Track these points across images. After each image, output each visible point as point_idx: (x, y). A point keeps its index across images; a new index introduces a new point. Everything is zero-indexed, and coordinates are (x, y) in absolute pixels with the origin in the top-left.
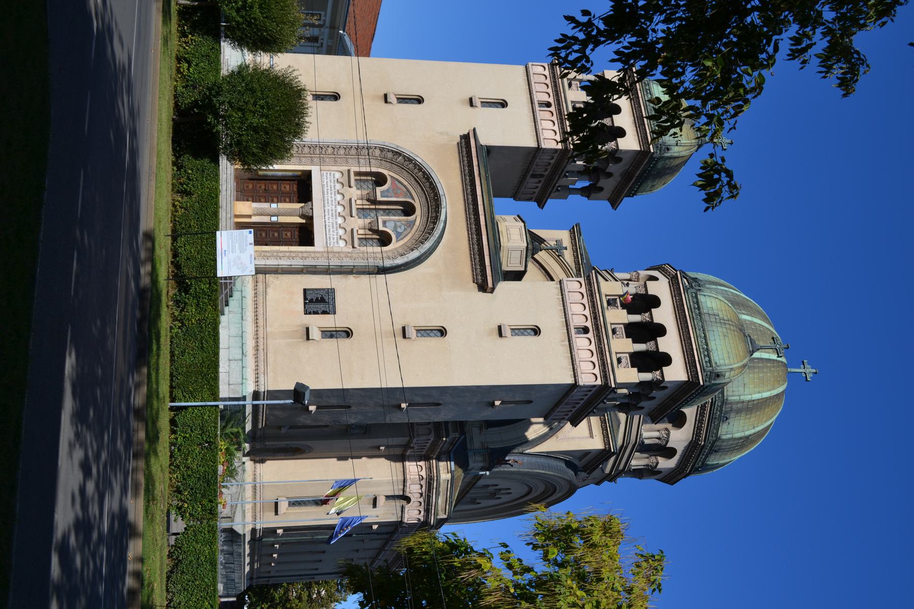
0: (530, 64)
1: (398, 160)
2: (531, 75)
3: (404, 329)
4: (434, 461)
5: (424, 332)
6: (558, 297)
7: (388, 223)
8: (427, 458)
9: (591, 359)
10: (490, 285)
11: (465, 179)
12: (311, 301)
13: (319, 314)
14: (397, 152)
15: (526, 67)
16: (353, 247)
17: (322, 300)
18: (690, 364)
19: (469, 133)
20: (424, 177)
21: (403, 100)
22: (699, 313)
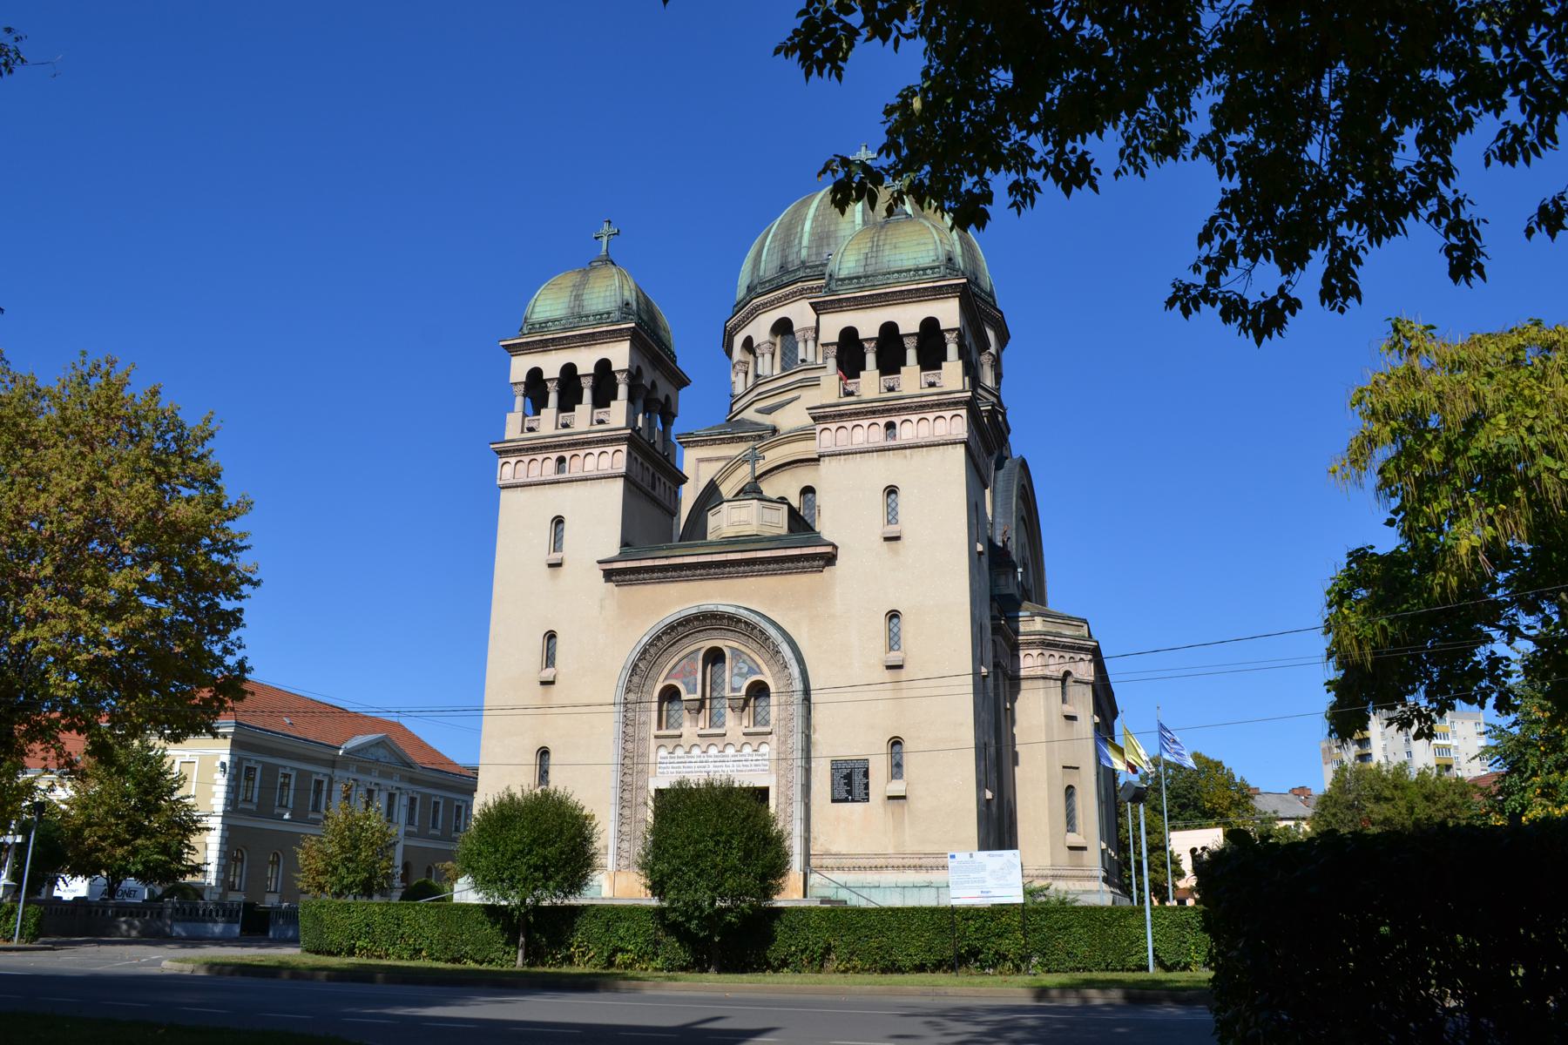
0: (498, 482)
1: (643, 668)
2: (515, 481)
3: (889, 667)
4: (1020, 638)
5: (893, 641)
6: (842, 461)
7: (734, 682)
8: (1015, 648)
9: (834, 431)
10: (829, 549)
11: (672, 577)
12: (849, 792)
13: (868, 783)
14: (633, 670)
15: (503, 488)
16: (771, 733)
17: (848, 778)
18: (936, 293)
19: (604, 570)
20: (669, 634)
21: (550, 659)
22: (865, 277)
